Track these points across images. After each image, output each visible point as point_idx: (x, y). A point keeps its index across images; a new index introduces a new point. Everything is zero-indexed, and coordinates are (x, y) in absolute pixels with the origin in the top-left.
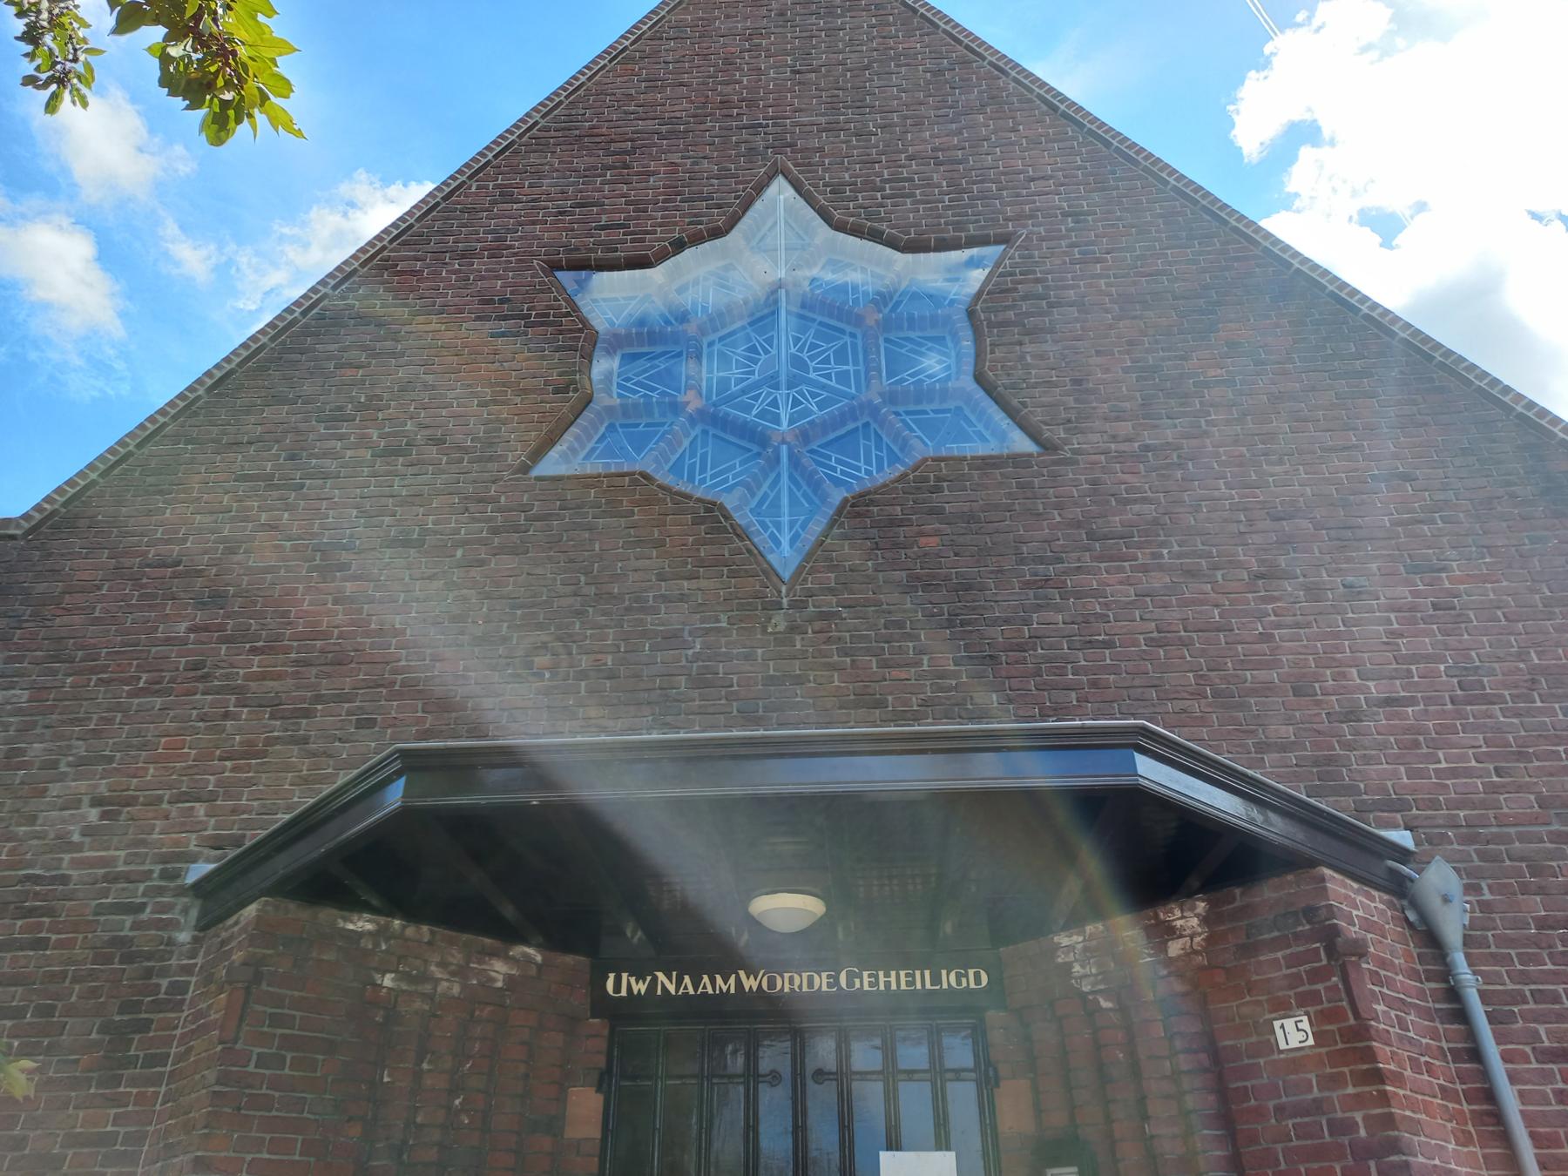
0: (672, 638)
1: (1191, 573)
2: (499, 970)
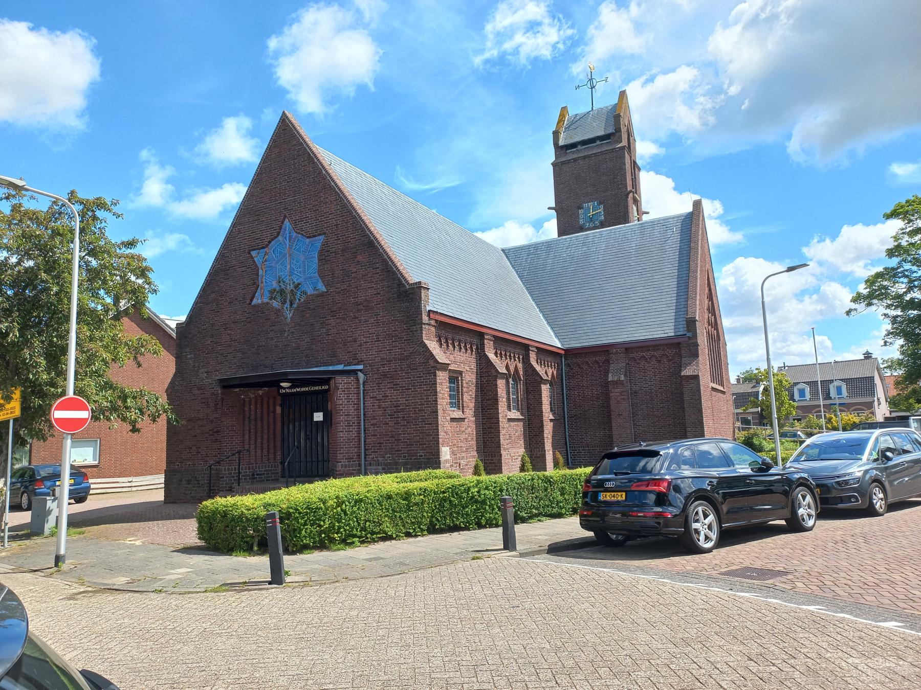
0: (272, 339)
1: (343, 319)
2: (260, 392)
